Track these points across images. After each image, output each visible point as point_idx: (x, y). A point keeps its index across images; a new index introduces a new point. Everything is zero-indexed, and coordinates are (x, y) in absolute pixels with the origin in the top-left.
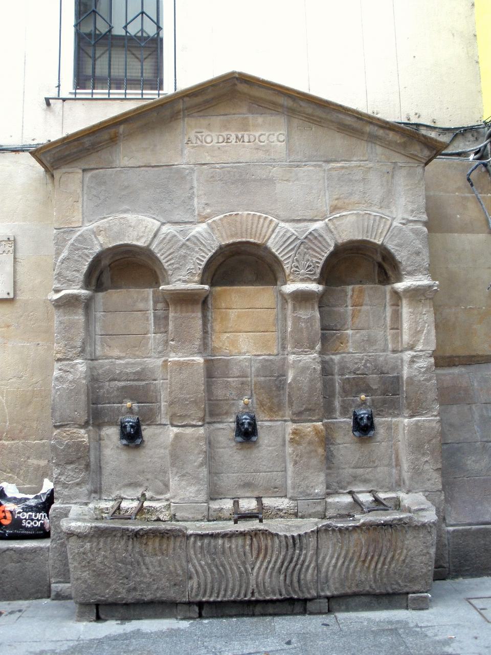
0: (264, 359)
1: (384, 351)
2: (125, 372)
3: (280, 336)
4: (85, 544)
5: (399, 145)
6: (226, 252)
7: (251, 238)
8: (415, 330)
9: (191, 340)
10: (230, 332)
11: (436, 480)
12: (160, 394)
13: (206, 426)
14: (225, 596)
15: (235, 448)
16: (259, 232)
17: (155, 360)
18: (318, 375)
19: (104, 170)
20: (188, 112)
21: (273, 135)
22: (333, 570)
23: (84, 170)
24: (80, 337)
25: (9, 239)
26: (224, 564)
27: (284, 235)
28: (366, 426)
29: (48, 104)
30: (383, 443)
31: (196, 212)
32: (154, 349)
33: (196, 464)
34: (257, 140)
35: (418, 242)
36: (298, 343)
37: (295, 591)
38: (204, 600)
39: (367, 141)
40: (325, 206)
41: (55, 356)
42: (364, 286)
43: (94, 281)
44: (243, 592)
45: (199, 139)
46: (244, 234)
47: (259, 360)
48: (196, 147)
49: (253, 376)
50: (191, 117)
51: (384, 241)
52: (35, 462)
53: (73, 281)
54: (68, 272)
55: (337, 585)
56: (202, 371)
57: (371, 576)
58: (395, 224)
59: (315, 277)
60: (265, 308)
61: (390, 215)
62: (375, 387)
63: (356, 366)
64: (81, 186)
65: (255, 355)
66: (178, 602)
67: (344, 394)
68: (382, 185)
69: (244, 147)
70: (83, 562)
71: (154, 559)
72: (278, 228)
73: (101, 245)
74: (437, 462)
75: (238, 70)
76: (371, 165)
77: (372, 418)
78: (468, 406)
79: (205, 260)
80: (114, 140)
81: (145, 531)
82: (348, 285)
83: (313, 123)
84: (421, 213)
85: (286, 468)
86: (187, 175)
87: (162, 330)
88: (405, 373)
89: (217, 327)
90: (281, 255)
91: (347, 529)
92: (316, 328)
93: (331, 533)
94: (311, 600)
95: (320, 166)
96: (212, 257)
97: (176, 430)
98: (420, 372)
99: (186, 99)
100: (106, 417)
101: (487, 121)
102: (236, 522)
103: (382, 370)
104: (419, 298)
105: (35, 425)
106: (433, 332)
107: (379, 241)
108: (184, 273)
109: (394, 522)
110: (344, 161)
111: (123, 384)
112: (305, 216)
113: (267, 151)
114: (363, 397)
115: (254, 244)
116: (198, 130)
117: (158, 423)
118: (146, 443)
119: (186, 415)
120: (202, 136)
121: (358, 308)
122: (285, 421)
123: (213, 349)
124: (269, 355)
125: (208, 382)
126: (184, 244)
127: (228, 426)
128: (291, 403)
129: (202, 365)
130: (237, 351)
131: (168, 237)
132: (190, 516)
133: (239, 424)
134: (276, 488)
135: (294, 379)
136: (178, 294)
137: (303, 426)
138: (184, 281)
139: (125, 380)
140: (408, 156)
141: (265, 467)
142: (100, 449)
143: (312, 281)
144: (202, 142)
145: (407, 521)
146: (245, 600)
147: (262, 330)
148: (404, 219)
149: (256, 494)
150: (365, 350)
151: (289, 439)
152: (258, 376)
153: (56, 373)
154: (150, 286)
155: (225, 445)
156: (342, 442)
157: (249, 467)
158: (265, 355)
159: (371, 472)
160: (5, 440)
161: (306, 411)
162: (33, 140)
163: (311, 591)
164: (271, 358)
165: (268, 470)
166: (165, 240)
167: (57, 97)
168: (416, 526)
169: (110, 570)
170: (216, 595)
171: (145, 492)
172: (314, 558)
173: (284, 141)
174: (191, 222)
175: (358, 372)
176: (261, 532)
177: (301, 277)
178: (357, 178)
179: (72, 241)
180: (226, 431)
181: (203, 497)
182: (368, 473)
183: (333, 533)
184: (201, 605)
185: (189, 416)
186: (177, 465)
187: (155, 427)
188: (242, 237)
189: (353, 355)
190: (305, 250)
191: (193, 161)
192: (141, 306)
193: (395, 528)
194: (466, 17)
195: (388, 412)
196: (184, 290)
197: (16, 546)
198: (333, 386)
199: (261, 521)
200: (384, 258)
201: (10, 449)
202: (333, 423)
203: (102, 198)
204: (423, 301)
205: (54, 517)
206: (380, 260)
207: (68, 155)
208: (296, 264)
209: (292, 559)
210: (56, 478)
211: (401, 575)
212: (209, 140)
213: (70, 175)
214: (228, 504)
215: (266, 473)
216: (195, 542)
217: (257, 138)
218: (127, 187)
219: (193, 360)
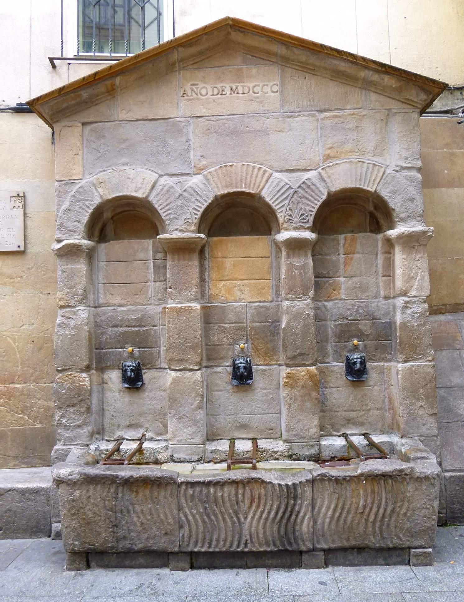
0: (259, 305)
1: (376, 297)
2: (127, 318)
3: (274, 283)
4: (75, 490)
5: (395, 89)
6: (222, 204)
7: (245, 188)
8: (409, 276)
9: (187, 287)
10: (227, 280)
11: (432, 425)
12: (160, 339)
13: (204, 370)
14: (216, 546)
15: (231, 391)
16: (253, 182)
17: (156, 306)
18: (311, 321)
20: (183, 64)
21: (267, 85)
22: (330, 523)
23: (84, 124)
25: (18, 195)
26: (216, 513)
27: (277, 185)
28: (359, 370)
29: (54, 66)
30: (376, 387)
31: (193, 165)
32: (154, 296)
34: (251, 91)
35: (411, 189)
36: (291, 290)
37: (290, 544)
38: (196, 550)
39: (360, 88)
40: (318, 155)
41: (58, 304)
42: (356, 235)
43: (97, 233)
44: (236, 543)
45: (195, 92)
46: (239, 185)
47: (255, 306)
48: (192, 100)
50: (186, 70)
51: (378, 188)
53: (74, 232)
54: (69, 223)
58: (388, 171)
59: (308, 225)
60: (260, 257)
61: (383, 162)
64: (81, 139)
65: (250, 302)
66: (169, 551)
70: (73, 509)
72: (272, 178)
73: (101, 197)
74: (433, 406)
75: (232, 16)
76: (364, 113)
79: (202, 210)
80: (111, 92)
82: (340, 234)
83: (306, 72)
86: (183, 128)
88: (399, 319)
89: (214, 275)
92: (309, 275)
93: (327, 483)
95: (314, 116)
96: (208, 206)
97: (173, 374)
98: (413, 317)
99: (180, 49)
100: (109, 361)
103: (374, 316)
104: (413, 245)
106: (427, 278)
107: (371, 188)
110: (337, 109)
111: (124, 329)
112: (298, 166)
113: (261, 102)
114: (355, 342)
115: (249, 194)
116: (193, 83)
118: (146, 386)
119: (184, 359)
120: (197, 88)
121: (351, 256)
123: (211, 296)
124: (264, 302)
125: (205, 327)
126: (181, 195)
127: (226, 369)
128: (285, 347)
129: (199, 311)
130: (233, 298)
131: (165, 189)
132: (187, 457)
133: (235, 367)
134: (272, 430)
135: (288, 325)
136: (175, 242)
137: (296, 370)
138: (181, 231)
139: (126, 326)
140: (403, 102)
141: (260, 410)
143: (306, 229)
144: (197, 94)
145: (407, 472)
146: (238, 551)
147: (257, 278)
148: (397, 166)
149: (251, 435)
150: (357, 296)
151: (283, 383)
152: (253, 322)
153: (59, 320)
155: (222, 388)
156: (336, 385)
158: (260, 302)
159: (364, 415)
160: (17, 383)
164: (266, 304)
165: (263, 412)
166: (162, 192)
167: (60, 57)
168: (418, 477)
170: (208, 545)
171: (146, 433)
172: (310, 509)
173: (277, 91)
174: (188, 174)
177: (294, 225)
178: (351, 126)
179: (73, 193)
180: (222, 375)
181: (198, 439)
182: (361, 416)
184: (192, 554)
185: (186, 361)
187: (155, 370)
188: (237, 187)
189: (346, 301)
190: (299, 199)
191: (188, 114)
192: (141, 256)
193: (395, 479)
195: (380, 357)
196: (181, 238)
200: (376, 207)
201: (22, 391)
202: (327, 367)
203: (102, 151)
204: (416, 247)
205: (56, 458)
206: (371, 208)
207: (67, 108)
208: (290, 213)
210: (58, 420)
212: (204, 92)
214: (224, 446)
215: (262, 415)
216: (186, 490)
218: (125, 141)
219: (190, 307)
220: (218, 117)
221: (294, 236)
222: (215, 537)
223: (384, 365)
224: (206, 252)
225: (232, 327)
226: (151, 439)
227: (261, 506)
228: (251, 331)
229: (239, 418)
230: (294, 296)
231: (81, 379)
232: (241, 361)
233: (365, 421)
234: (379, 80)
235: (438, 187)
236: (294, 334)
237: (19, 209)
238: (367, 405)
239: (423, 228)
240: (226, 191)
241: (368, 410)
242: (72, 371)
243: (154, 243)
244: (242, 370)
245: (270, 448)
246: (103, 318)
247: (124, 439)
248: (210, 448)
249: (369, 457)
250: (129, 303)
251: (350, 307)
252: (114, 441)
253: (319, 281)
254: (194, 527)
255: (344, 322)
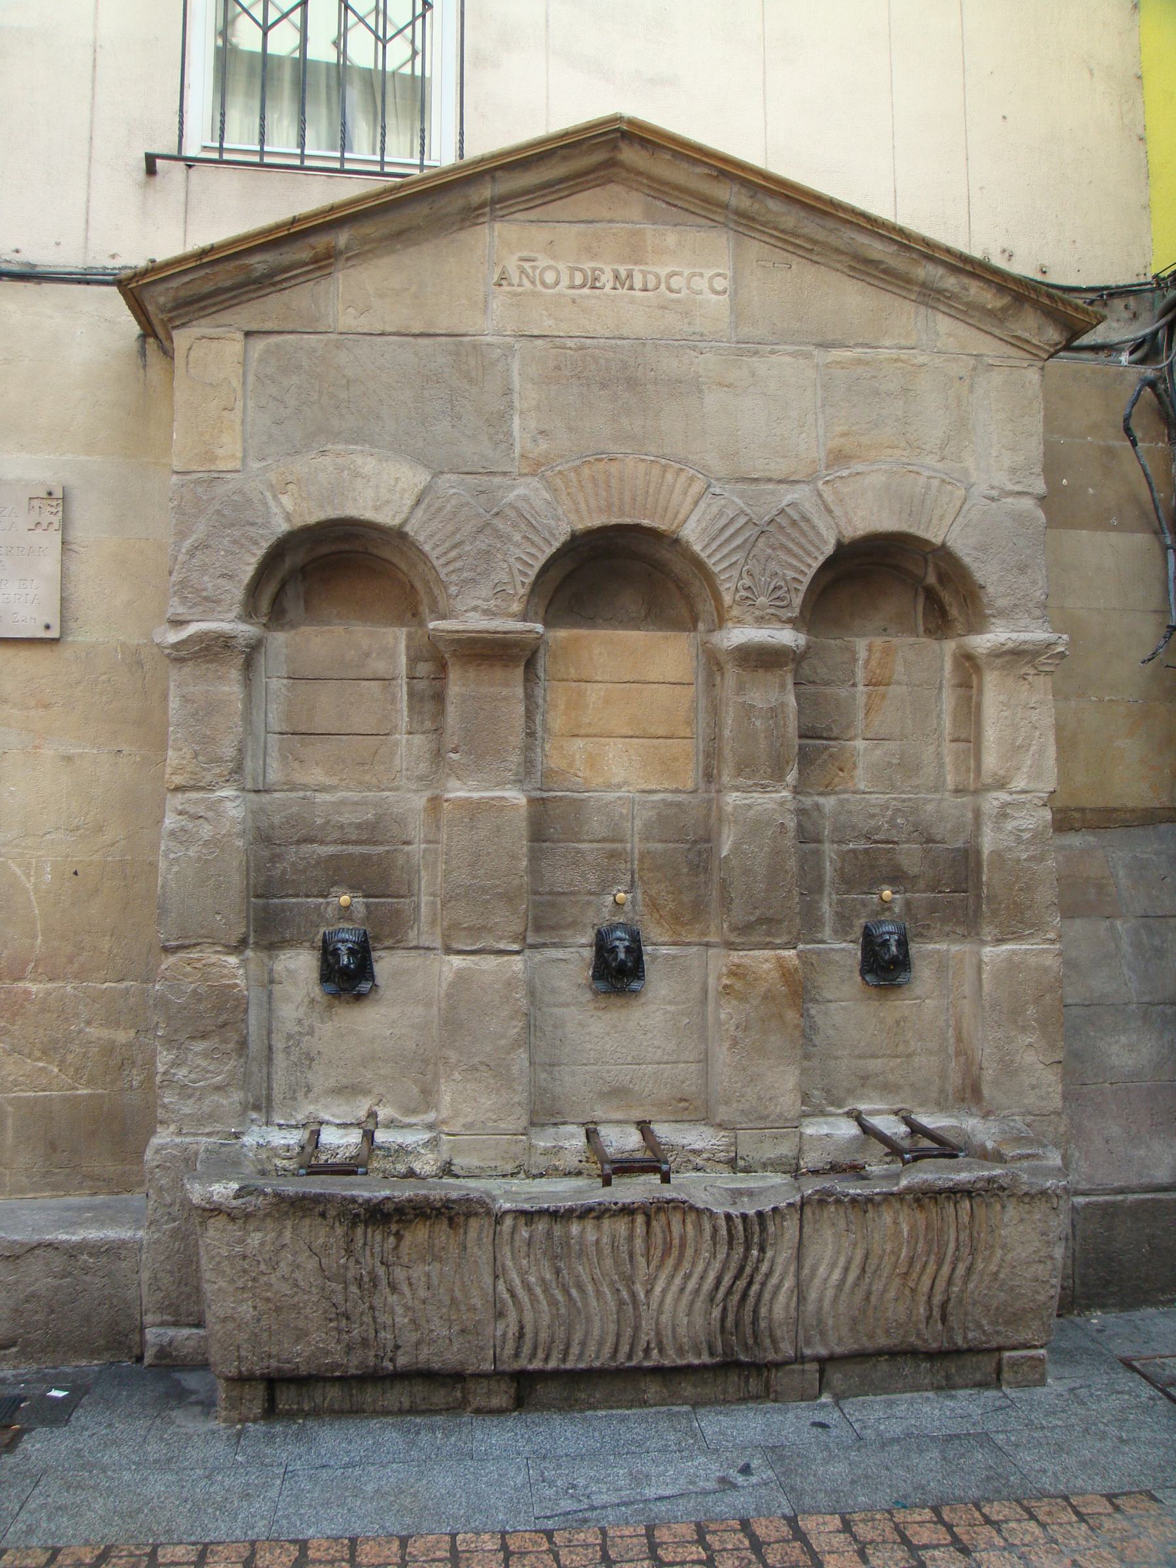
0: (663, 800)
1: (936, 789)
2: (338, 822)
3: (701, 747)
10: (587, 736)
13: (527, 952)
15: (592, 1006)
18: (789, 841)
19: (299, 336)
21: (701, 275)
22: (836, 1298)
23: (248, 334)
24: (231, 736)
25: (50, 494)
27: (721, 513)
30: (927, 1001)
32: (407, 769)
33: (503, 1042)
34: (663, 286)
36: (744, 766)
37: (746, 1348)
42: (895, 641)
43: (265, 604)
44: (625, 1348)
49: (636, 839)
50: (508, 221)
52: (105, 1033)
53: (218, 602)
54: (206, 578)
55: (844, 1331)
56: (523, 826)
57: (922, 1310)
62: (914, 871)
63: (872, 823)
67: (843, 887)
68: (947, 407)
69: (632, 301)
71: (418, 1272)
73: (288, 517)
76: (922, 359)
77: (906, 944)
78: (1108, 923)
79: (538, 565)
80: (325, 262)
81: (397, 1203)
84: (1033, 477)
85: (707, 1053)
87: (428, 724)
88: (988, 842)
89: (557, 722)
90: (713, 560)
91: (869, 1200)
93: (833, 1209)
94: (778, 1365)
95: (808, 356)
97: (457, 961)
98: (1019, 840)
101: (1162, 275)
102: (607, 1182)
103: (929, 834)
105: (106, 944)
106: (1052, 751)
108: (485, 592)
109: (979, 1185)
111: (331, 849)
114: (887, 893)
116: (525, 254)
117: (411, 945)
118: (381, 992)
119: (484, 927)
120: (534, 268)
122: (708, 945)
123: (548, 774)
124: (677, 791)
129: (523, 812)
130: (601, 780)
133: (602, 946)
134: (686, 1100)
135: (736, 849)
137: (753, 957)
138: (486, 612)
139: (335, 842)
141: (659, 1052)
142: (270, 1003)
144: (533, 283)
145: (1004, 1182)
147: (660, 733)
149: (638, 1114)
150: (892, 786)
152: (647, 839)
153: (171, 821)
154: (400, 621)
155: (569, 1000)
157: (624, 1050)
158: (666, 791)
161: (762, 924)
162: (113, 256)
163: (782, 1345)
164: (681, 797)
167: (175, 153)
169: (306, 1297)
171: (376, 1108)
172: (792, 1269)
173: (725, 292)
175: (876, 837)
176: (671, 1205)
177: (758, 613)
182: (892, 1070)
183: (836, 1210)
186: (457, 1044)
189: (867, 796)
190: (769, 551)
192: (379, 666)
194: (1120, 33)
197: (60, 1237)
198: (819, 868)
199: (666, 1179)
202: (818, 953)
204: (1030, 678)
205: (157, 1167)
206: (931, 579)
208: (747, 581)
209: (741, 1270)
211: (987, 1308)
212: (550, 277)
213: (215, 344)
215: (662, 1066)
216: (514, 1229)
217: (663, 280)
219: (503, 798)
220: (583, 340)
221: (756, 639)
222: (577, 1337)
223: (948, 951)
224: (539, 666)
225: (598, 850)
226: (391, 1124)
227: (686, 1265)
228: (641, 860)
229: (608, 1072)
230: (751, 782)
231: (225, 971)
232: (619, 934)
233: (902, 1082)
234: (956, 289)
235: (1073, 527)
236: (746, 872)
237: (52, 529)
238: (906, 1043)
239: (1046, 635)
240: (597, 521)
241: (909, 1056)
242: (201, 951)
243: (410, 637)
244: (622, 956)
245: (685, 1142)
246: (277, 819)
247: (321, 1123)
248: (542, 1144)
249: (920, 1155)
250: (344, 784)
251: (877, 810)
252: (296, 1127)
253: (807, 745)
254: (528, 1317)
255: (862, 845)
